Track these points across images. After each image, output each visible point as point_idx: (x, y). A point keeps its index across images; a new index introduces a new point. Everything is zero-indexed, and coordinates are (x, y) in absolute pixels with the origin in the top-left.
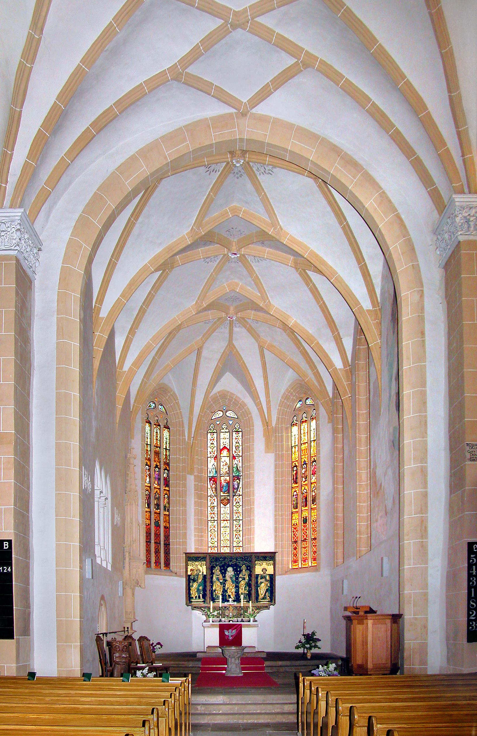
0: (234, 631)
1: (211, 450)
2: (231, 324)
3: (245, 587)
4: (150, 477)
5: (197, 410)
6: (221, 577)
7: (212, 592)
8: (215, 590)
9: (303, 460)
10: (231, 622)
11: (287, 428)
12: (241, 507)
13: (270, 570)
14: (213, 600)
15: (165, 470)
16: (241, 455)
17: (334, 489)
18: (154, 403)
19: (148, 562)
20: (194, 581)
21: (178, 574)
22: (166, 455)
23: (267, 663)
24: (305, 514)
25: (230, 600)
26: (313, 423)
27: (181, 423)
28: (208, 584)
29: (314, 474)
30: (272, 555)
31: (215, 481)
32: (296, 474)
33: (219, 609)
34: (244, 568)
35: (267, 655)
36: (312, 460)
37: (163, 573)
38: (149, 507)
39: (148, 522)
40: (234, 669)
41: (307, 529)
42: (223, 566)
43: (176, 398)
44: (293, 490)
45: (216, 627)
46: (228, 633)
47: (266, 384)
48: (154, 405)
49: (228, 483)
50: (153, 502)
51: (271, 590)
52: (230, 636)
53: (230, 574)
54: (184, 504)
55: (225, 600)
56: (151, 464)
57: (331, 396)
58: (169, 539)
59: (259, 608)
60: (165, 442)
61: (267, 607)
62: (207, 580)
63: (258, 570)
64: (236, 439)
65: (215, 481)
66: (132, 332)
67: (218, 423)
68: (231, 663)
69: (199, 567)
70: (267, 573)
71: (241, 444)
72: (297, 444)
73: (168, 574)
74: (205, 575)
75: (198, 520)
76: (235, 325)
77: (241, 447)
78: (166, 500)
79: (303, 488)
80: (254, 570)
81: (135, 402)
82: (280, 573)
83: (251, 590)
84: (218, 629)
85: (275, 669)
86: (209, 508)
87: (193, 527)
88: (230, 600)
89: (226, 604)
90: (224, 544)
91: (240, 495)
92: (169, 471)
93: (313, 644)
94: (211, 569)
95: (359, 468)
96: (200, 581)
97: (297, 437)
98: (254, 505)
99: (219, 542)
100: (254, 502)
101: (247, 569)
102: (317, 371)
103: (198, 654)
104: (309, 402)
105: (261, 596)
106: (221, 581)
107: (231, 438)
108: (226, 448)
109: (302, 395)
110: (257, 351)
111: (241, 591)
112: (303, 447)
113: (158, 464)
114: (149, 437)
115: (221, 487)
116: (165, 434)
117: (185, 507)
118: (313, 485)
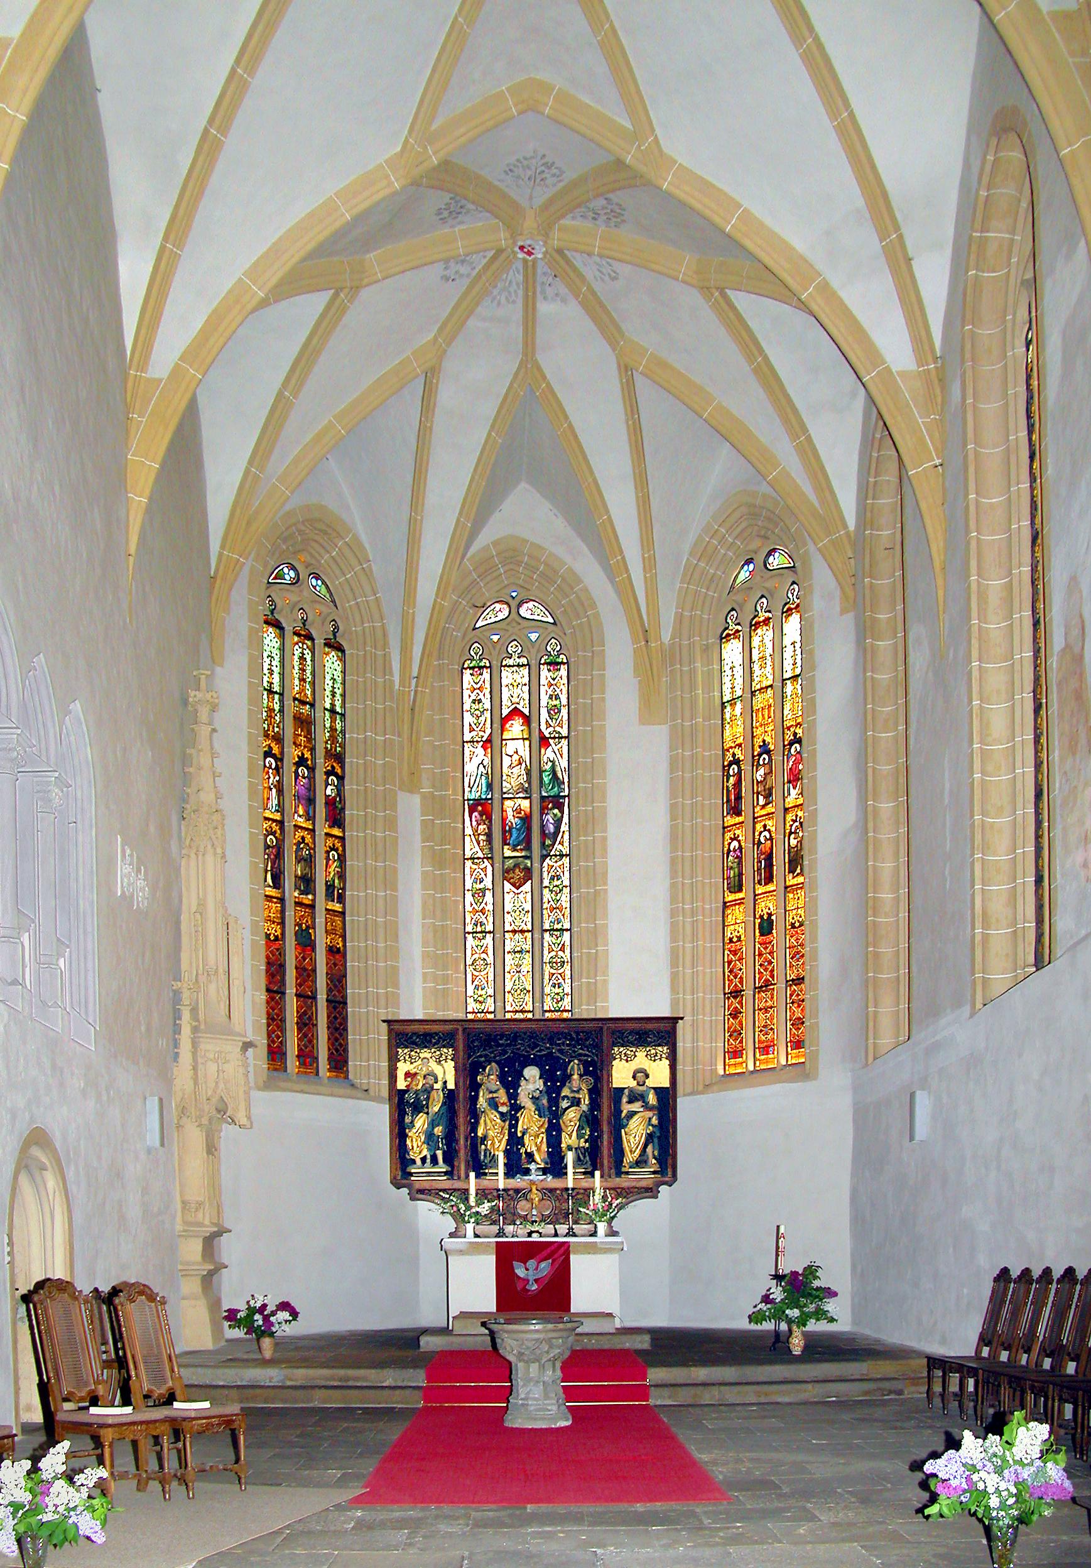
0: (543, 1265)
1: (475, 722)
2: (529, 270)
3: (581, 1128)
4: (280, 792)
7: (475, 1143)
8: (484, 1138)
9: (758, 742)
10: (535, 1238)
11: (706, 649)
12: (566, 891)
13: (659, 1075)
14: (479, 1167)
15: (328, 774)
16: (564, 732)
17: (866, 817)
18: (293, 568)
19: (276, 1054)
20: (418, 1108)
21: (372, 1093)
22: (333, 729)
23: (655, 1374)
24: (767, 906)
25: (533, 1166)
26: (792, 626)
27: (379, 634)
28: (462, 1120)
29: (795, 778)
31: (487, 815)
32: (738, 784)
33: (498, 1194)
34: (575, 1067)
35: (653, 1340)
36: (789, 736)
37: (322, 1089)
38: (277, 882)
40: (538, 1401)
41: (771, 953)
42: (509, 1062)
43: (362, 559)
44: (728, 835)
45: (485, 1252)
46: (528, 1272)
48: (292, 574)
49: (527, 820)
50: (292, 868)
51: (664, 1137)
52: (534, 1285)
53: (531, 1087)
54: (390, 881)
55: (515, 1167)
56: (282, 753)
57: (851, 523)
59: (629, 1194)
60: (328, 689)
61: (651, 1192)
62: (460, 1107)
63: (621, 1074)
65: (487, 815)
66: (178, 230)
67: (495, 638)
70: (650, 1083)
71: (564, 701)
72: (739, 693)
73: (342, 1091)
75: (435, 932)
76: (543, 292)
77: (564, 712)
78: (334, 867)
79: (759, 827)
80: (610, 1075)
81: (223, 547)
82: (688, 1090)
83: (600, 1137)
84: (492, 1258)
85: (683, 1396)
86: (468, 895)
87: (417, 951)
88: (533, 1166)
89: (518, 1182)
91: (562, 856)
92: (341, 778)
93: (812, 1308)
94: (469, 1073)
95: (980, 693)
96: (436, 1109)
97: (738, 672)
98: (605, 884)
99: (499, 997)
100: (605, 874)
102: (809, 439)
103: (424, 1340)
104: (776, 561)
105: (630, 1157)
106: (504, 1109)
107: (534, 686)
108: (521, 714)
109: (756, 543)
110: (613, 385)
111: (566, 1141)
112: (760, 701)
113: (307, 755)
114: (276, 670)
115: (504, 831)
117: (395, 889)
118: (789, 817)
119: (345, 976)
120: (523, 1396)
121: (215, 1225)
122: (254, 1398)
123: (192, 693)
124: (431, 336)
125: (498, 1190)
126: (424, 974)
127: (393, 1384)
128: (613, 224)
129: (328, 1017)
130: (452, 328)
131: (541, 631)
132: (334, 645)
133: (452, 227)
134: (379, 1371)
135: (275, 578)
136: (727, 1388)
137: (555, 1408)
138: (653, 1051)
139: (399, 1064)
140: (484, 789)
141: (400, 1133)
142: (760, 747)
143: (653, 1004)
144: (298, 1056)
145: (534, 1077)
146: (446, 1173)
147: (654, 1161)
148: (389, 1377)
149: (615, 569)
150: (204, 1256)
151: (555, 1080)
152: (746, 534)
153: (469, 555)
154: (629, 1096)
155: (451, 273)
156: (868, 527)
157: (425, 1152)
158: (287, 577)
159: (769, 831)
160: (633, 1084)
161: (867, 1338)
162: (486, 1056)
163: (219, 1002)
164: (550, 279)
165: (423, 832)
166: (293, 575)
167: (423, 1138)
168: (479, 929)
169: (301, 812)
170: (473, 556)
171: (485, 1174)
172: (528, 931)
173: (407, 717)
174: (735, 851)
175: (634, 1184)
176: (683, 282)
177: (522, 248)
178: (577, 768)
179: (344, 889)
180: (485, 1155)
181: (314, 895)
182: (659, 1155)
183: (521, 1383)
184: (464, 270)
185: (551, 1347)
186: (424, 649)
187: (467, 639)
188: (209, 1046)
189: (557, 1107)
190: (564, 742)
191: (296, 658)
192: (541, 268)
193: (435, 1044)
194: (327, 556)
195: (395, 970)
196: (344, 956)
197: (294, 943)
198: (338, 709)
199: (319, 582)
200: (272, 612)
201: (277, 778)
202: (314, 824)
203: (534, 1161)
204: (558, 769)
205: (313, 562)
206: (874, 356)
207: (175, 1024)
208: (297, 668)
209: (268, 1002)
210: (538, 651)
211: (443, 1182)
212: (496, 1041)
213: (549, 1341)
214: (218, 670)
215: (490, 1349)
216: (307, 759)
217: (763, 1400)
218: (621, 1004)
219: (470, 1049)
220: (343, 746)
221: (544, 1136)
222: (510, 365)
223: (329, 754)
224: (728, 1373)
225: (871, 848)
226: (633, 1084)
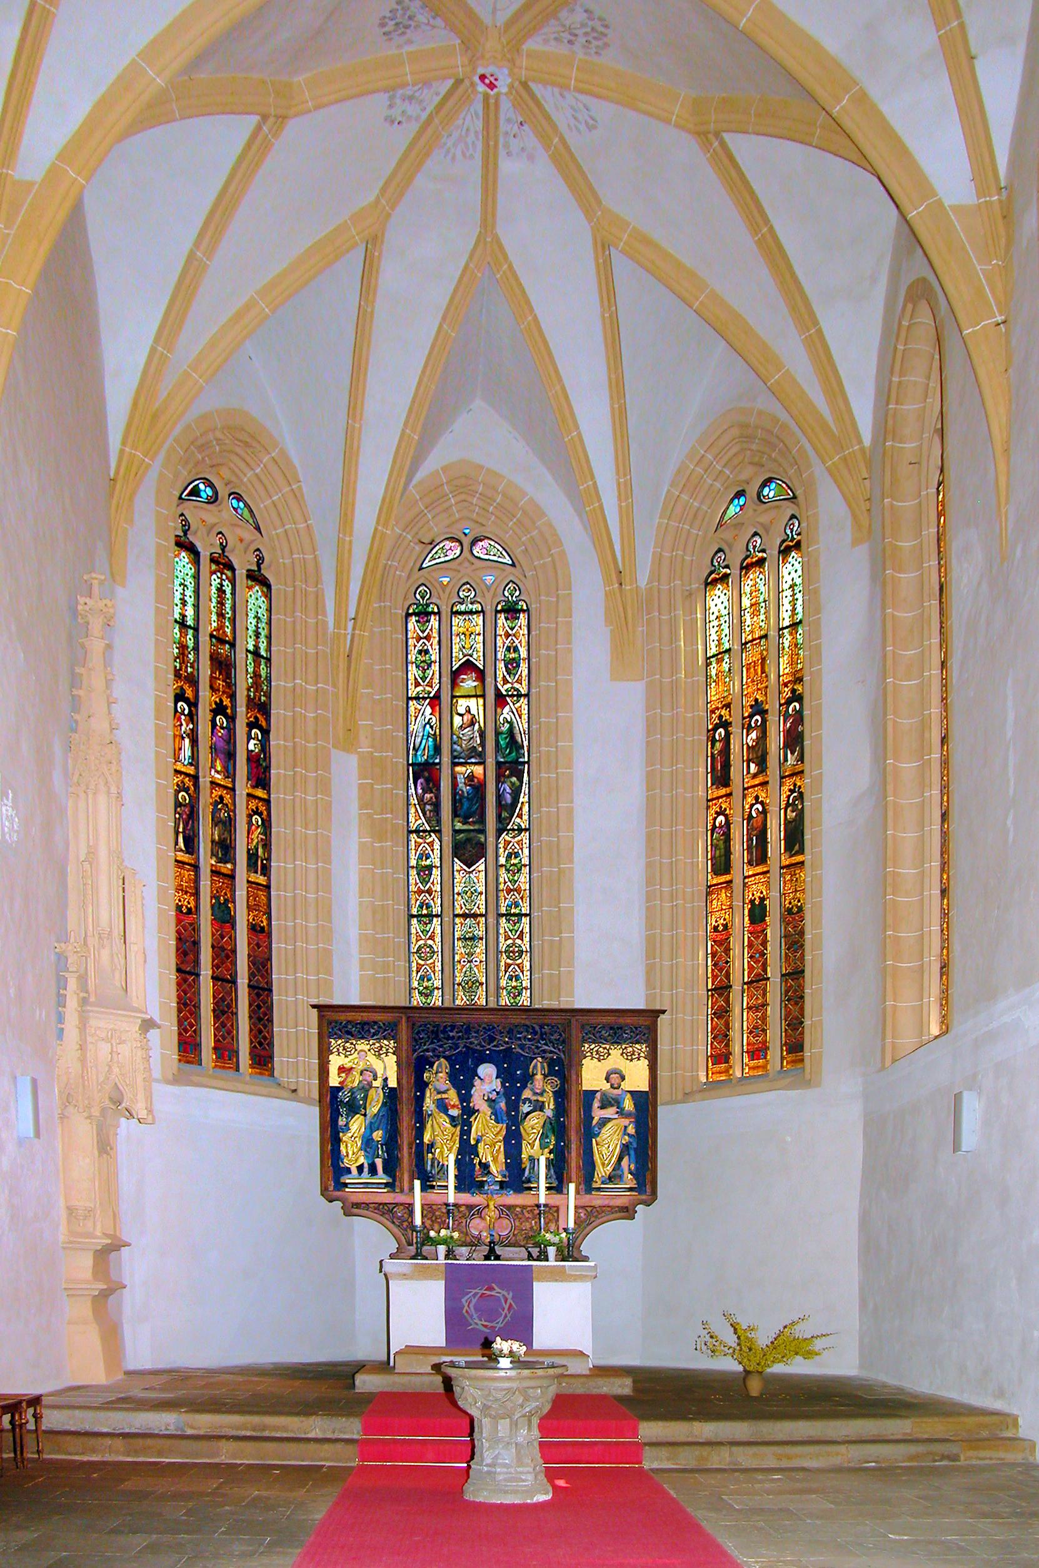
2: (490, 108)
3: (544, 1136)
4: (194, 743)
5: (365, 517)
6: (452, 1096)
7: (421, 1150)
8: (432, 1145)
13: (637, 1076)
17: (883, 779)
18: (209, 484)
19: (188, 1046)
20: (354, 1108)
21: (300, 1092)
22: (256, 675)
23: (649, 1430)
30: (641, 1021)
34: (538, 1066)
39: (188, 901)
47: (620, 417)
48: (209, 492)
50: (206, 833)
51: (643, 1149)
53: (487, 1088)
54: (322, 852)
55: (468, 1180)
56: (197, 696)
57: (867, 438)
58: (269, 972)
60: (252, 628)
61: (627, 1212)
62: (402, 1109)
63: (592, 1074)
64: (508, 635)
68: (495, 1440)
69: (372, 1059)
70: (626, 1086)
71: (523, 653)
74: (392, 1089)
75: (374, 912)
76: (506, 145)
78: (257, 835)
80: (579, 1075)
81: (124, 443)
83: (567, 1146)
84: (441, 1284)
85: (687, 1458)
90: (462, 977)
91: (520, 830)
92: (266, 732)
94: (416, 1069)
96: (375, 1110)
98: (571, 861)
99: (447, 989)
101: (551, 1073)
102: (820, 332)
103: (360, 1379)
105: (602, 1171)
106: (455, 1112)
113: (227, 702)
114: (190, 601)
115: (454, 801)
116: (251, 601)
117: (328, 860)
119: (270, 959)
120: (488, 1461)
121: (107, 1236)
122: (144, 1450)
123: (82, 600)
124: (372, 198)
125: (447, 1205)
126: (362, 960)
127: (320, 1436)
128: (593, 51)
129: (250, 1005)
130: (397, 186)
131: (498, 573)
132: (257, 577)
133: (400, 47)
134: (303, 1418)
135: (188, 495)
136: (741, 1449)
137: (530, 1477)
138: (630, 1049)
139: (331, 1057)
140: (432, 753)
141: (332, 1136)
142: (751, 706)
143: (630, 996)
144: (215, 1048)
145: (490, 1076)
146: (387, 1185)
147: (630, 1176)
148: (316, 1426)
149: (585, 498)
150: (95, 1274)
151: (514, 1080)
152: (736, 461)
153: (415, 481)
154: (602, 1101)
155: (396, 113)
156: (890, 437)
157: (362, 1160)
158: (203, 494)
159: (762, 803)
160: (606, 1086)
161: (884, 1386)
162: (434, 1050)
163: (113, 971)
164: (516, 127)
165: (360, 798)
166: (210, 493)
167: (359, 1144)
168: (425, 912)
169: (219, 768)
170: (421, 482)
171: (433, 1187)
172: (481, 915)
173: (343, 664)
174: (721, 827)
175: (606, 1202)
176: (677, 126)
177: (483, 78)
178: (539, 730)
179: (269, 859)
180: (432, 1165)
181: (235, 864)
182: (637, 1168)
183: (486, 1444)
184: (412, 110)
185: (527, 1399)
186: (362, 586)
187: (411, 580)
188: (100, 1023)
189: (517, 1111)
190: (523, 701)
191: (214, 590)
192: (506, 105)
193: (374, 1034)
194: (250, 474)
195: (328, 953)
196: (269, 935)
197: (210, 917)
198: (263, 653)
199: (241, 504)
200: (185, 533)
201: (191, 726)
202: (234, 782)
203: (489, 1173)
204: (516, 731)
205: (234, 479)
206: (924, 187)
207: (59, 995)
208: (214, 600)
209: (179, 984)
210: (494, 596)
211: (386, 1196)
212: (444, 1031)
213: (524, 1392)
214: (119, 590)
215: (441, 1390)
216: (226, 707)
217: (785, 1464)
218: (587, 994)
219: (416, 1041)
220: (268, 695)
221: (502, 1144)
222: (464, 240)
223: (251, 703)
224: (739, 1429)
225: (890, 814)
226: (606, 1086)
